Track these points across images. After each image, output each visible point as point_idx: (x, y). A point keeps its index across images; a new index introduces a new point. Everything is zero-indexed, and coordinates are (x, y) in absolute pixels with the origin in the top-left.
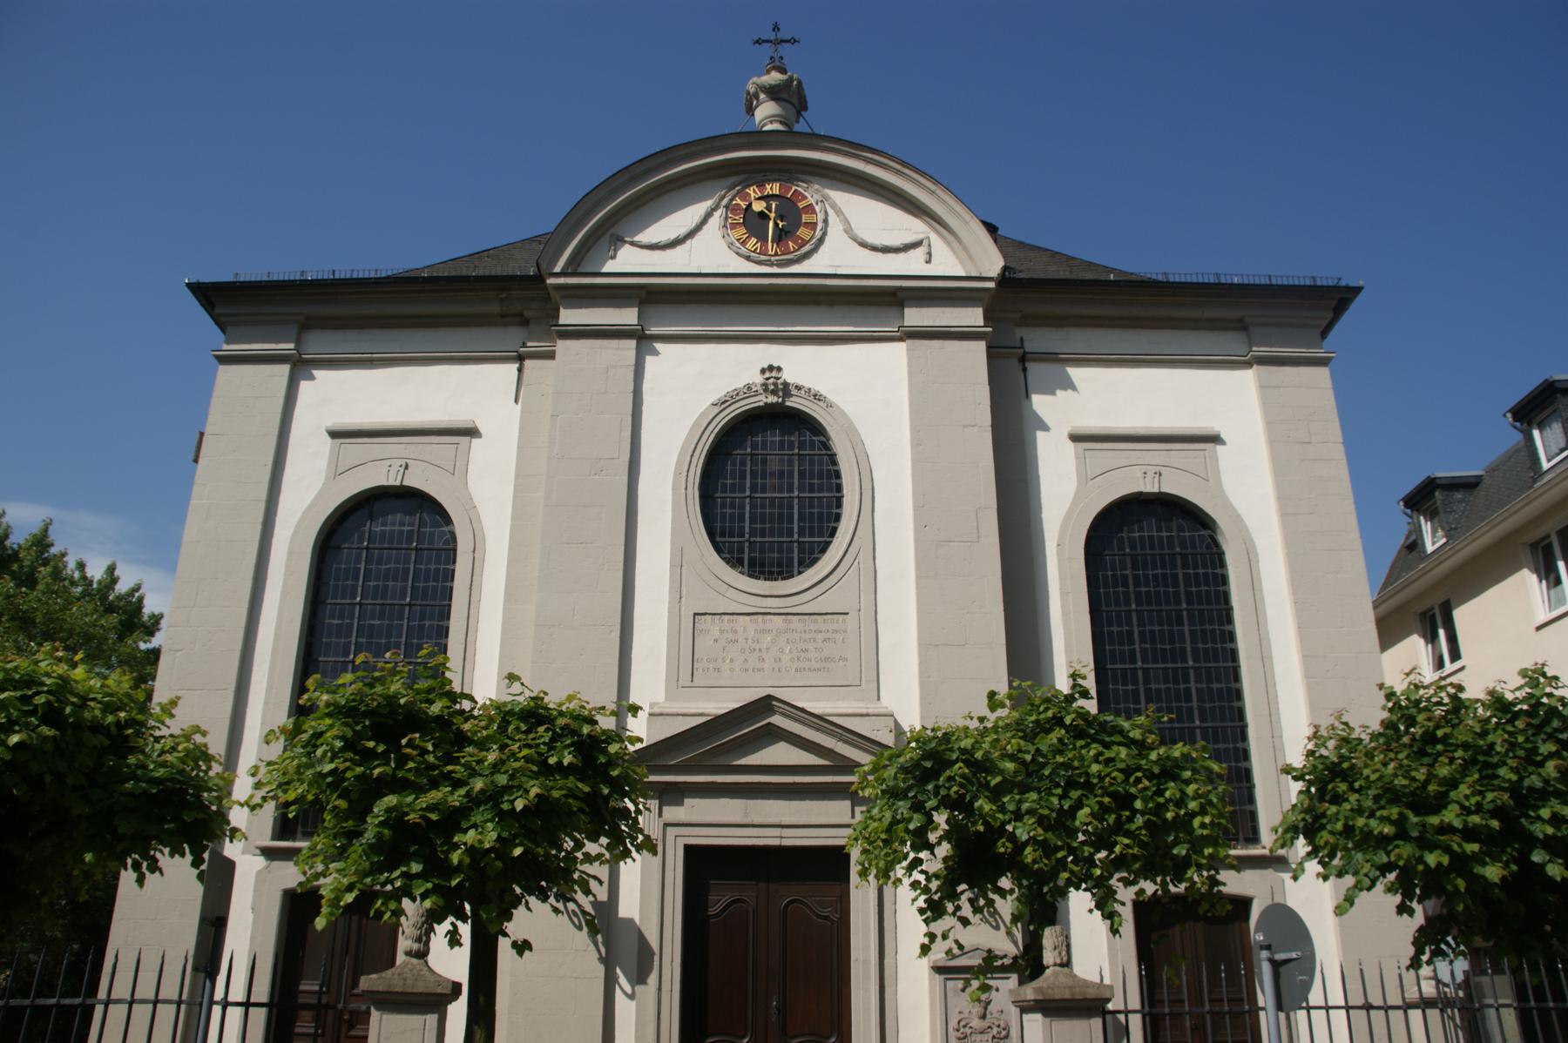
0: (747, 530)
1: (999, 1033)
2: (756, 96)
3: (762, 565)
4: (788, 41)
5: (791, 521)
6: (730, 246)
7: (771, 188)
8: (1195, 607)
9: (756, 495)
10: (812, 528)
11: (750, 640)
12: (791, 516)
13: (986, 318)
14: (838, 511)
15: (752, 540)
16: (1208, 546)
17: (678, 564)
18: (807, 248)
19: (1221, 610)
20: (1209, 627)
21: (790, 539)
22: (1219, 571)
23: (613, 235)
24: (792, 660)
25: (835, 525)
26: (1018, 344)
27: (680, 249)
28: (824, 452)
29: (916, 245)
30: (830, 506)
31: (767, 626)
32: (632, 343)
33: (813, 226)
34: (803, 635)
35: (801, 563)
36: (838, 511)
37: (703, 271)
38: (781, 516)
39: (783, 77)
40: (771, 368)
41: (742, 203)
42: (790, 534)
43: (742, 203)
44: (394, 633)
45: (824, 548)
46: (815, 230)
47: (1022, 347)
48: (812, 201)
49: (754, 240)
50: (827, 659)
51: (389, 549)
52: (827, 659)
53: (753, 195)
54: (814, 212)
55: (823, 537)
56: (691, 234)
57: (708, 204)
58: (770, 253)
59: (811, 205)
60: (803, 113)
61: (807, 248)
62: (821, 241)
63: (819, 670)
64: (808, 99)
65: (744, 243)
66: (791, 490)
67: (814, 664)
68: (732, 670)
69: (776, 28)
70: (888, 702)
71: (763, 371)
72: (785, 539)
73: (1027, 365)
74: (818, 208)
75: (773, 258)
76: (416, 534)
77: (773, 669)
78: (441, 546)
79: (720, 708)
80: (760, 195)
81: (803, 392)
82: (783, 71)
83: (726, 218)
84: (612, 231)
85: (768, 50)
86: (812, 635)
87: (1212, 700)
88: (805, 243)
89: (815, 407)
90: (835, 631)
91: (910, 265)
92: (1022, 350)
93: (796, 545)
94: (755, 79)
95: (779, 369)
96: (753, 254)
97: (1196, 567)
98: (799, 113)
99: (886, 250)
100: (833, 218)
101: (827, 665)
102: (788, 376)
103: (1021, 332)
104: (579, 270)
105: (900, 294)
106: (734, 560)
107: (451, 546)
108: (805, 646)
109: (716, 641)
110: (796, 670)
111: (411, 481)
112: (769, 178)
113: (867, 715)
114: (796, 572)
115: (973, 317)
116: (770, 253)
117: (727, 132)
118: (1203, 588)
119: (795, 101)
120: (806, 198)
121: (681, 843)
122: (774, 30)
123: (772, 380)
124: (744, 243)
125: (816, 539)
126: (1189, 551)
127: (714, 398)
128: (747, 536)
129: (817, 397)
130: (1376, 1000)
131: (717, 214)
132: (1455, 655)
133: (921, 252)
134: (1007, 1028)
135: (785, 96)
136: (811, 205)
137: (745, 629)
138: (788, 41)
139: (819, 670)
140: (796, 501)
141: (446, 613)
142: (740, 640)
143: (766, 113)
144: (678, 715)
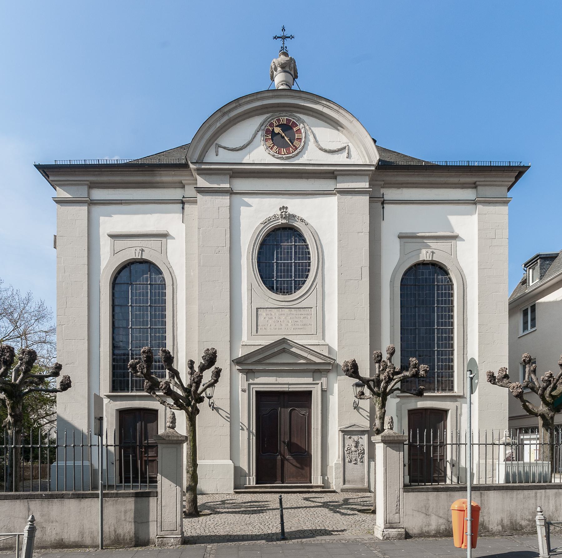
0: (275, 276)
1: (361, 452)
2: (276, 69)
3: (281, 289)
5: (291, 272)
8: (440, 306)
9: (278, 262)
10: (299, 275)
11: (277, 318)
12: (291, 269)
16: (448, 282)
17: (251, 289)
18: (291, 155)
19: (450, 307)
20: (444, 313)
21: (291, 279)
22: (450, 292)
23: (216, 144)
24: (292, 325)
26: (382, 197)
28: (304, 244)
30: (306, 266)
31: (283, 313)
34: (296, 316)
35: (295, 289)
36: (309, 268)
38: (288, 269)
39: (288, 59)
42: (291, 277)
43: (270, 128)
44: (9, 442)
46: (301, 142)
47: (383, 198)
50: (304, 325)
51: (140, 284)
52: (304, 325)
53: (275, 124)
61: (291, 155)
63: (302, 329)
66: (291, 260)
67: (300, 327)
68: (270, 329)
69: (283, 29)
70: (327, 341)
71: (280, 209)
72: (289, 279)
73: (385, 205)
75: (284, 156)
76: (149, 278)
78: (159, 283)
79: (267, 343)
82: (286, 54)
84: (215, 142)
85: (279, 42)
86: (300, 316)
87: (442, 341)
89: (301, 225)
90: (308, 314)
91: (340, 159)
92: (383, 199)
93: (293, 281)
95: (287, 208)
96: (275, 154)
97: (442, 290)
98: (294, 79)
101: (305, 327)
102: (290, 211)
103: (383, 191)
105: (335, 172)
106: (271, 288)
107: (163, 283)
110: (294, 329)
111: (145, 256)
113: (319, 345)
114: (293, 292)
115: (365, 185)
118: (444, 298)
119: (292, 73)
121: (254, 390)
122: (282, 30)
125: (301, 279)
126: (440, 284)
127: (262, 221)
128: (275, 278)
129: (302, 220)
130: (490, 447)
132: (533, 325)
133: (345, 154)
134: (364, 450)
135: (287, 69)
137: (275, 314)
139: (302, 329)
140: (293, 264)
141: (164, 309)
142: (273, 318)
143: (279, 78)
144: (252, 345)
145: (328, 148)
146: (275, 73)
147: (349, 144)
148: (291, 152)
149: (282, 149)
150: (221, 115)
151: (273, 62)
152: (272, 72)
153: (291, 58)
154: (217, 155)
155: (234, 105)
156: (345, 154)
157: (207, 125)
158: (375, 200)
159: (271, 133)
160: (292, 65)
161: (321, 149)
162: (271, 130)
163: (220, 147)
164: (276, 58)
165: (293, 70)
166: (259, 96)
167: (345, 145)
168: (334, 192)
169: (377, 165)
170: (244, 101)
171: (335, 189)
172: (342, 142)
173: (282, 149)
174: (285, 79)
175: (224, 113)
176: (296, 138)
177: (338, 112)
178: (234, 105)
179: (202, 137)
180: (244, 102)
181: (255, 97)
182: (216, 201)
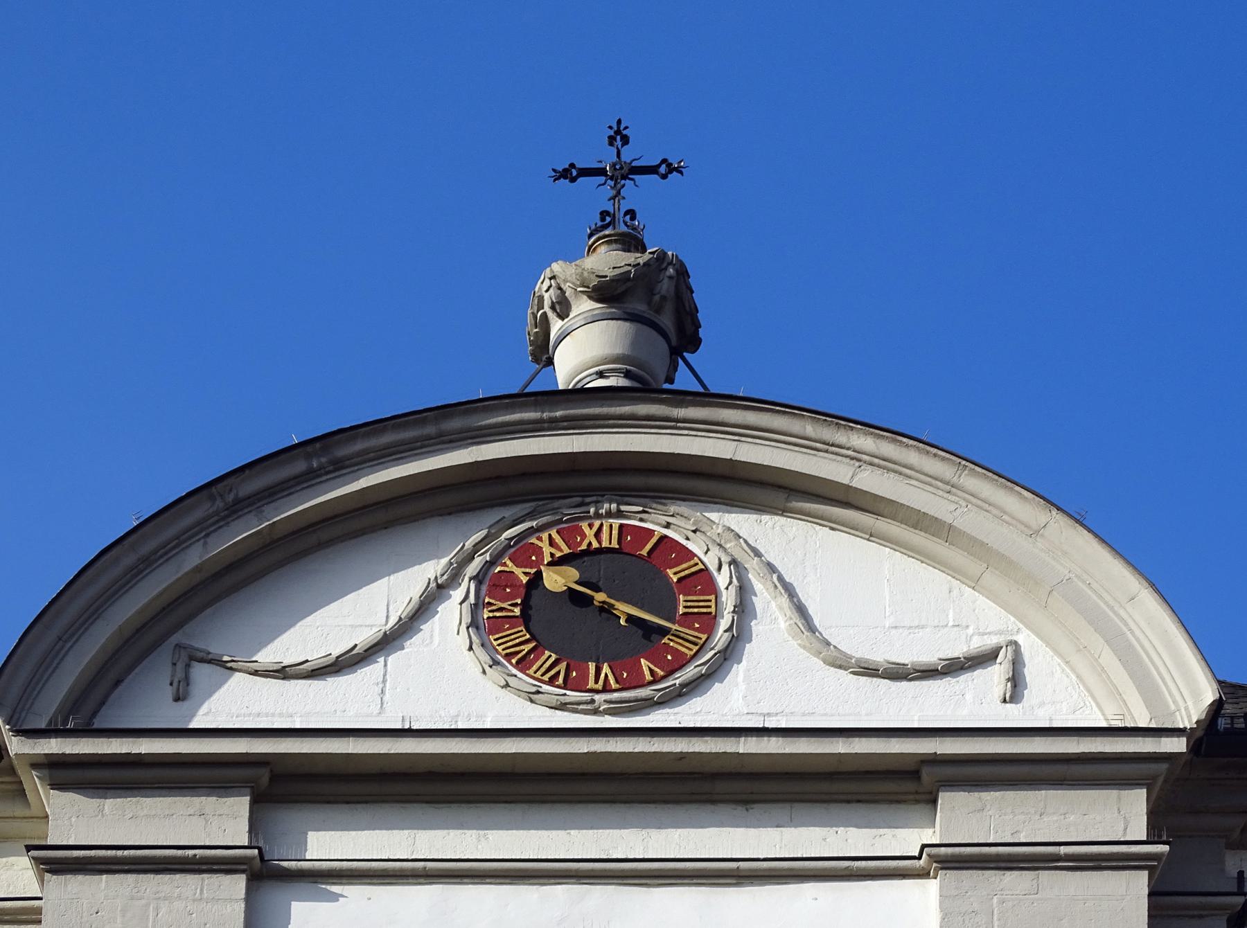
7: (598, 535)
13: (1153, 815)
18: (689, 672)
27: (369, 674)
32: (237, 885)
33: (709, 622)
41: (518, 571)
43: (518, 571)
53: (547, 550)
56: (387, 642)
57: (432, 569)
58: (591, 684)
61: (689, 672)
62: (729, 654)
69: (619, 136)
75: (597, 697)
80: (566, 550)
82: (631, 242)
83: (475, 609)
85: (597, 194)
88: (681, 662)
99: (898, 673)
100: (766, 599)
104: (97, 724)
116: (591, 684)
120: (692, 555)
122: (612, 140)
131: (457, 594)
133: (996, 675)
145: (879, 655)
146: (556, 326)
147: (1020, 639)
148: (648, 677)
149: (592, 667)
150: (217, 513)
151: (548, 273)
152: (545, 324)
153: (661, 257)
154: (177, 699)
155: (299, 466)
156: (996, 675)
157: (129, 560)
158: (1187, 907)
159: (523, 591)
160: (665, 287)
161: (840, 662)
162: (525, 579)
163: (202, 661)
164: (570, 258)
165: (669, 308)
166: (456, 423)
167: (991, 641)
168: (922, 862)
169: (1199, 733)
170: (359, 446)
171: (924, 846)
172: (970, 631)
173: (592, 667)
174: (618, 350)
175: (238, 501)
176: (681, 610)
177: (830, 447)
178: (299, 466)
179: (94, 613)
180: (359, 454)
181: (430, 430)
182: (157, 910)
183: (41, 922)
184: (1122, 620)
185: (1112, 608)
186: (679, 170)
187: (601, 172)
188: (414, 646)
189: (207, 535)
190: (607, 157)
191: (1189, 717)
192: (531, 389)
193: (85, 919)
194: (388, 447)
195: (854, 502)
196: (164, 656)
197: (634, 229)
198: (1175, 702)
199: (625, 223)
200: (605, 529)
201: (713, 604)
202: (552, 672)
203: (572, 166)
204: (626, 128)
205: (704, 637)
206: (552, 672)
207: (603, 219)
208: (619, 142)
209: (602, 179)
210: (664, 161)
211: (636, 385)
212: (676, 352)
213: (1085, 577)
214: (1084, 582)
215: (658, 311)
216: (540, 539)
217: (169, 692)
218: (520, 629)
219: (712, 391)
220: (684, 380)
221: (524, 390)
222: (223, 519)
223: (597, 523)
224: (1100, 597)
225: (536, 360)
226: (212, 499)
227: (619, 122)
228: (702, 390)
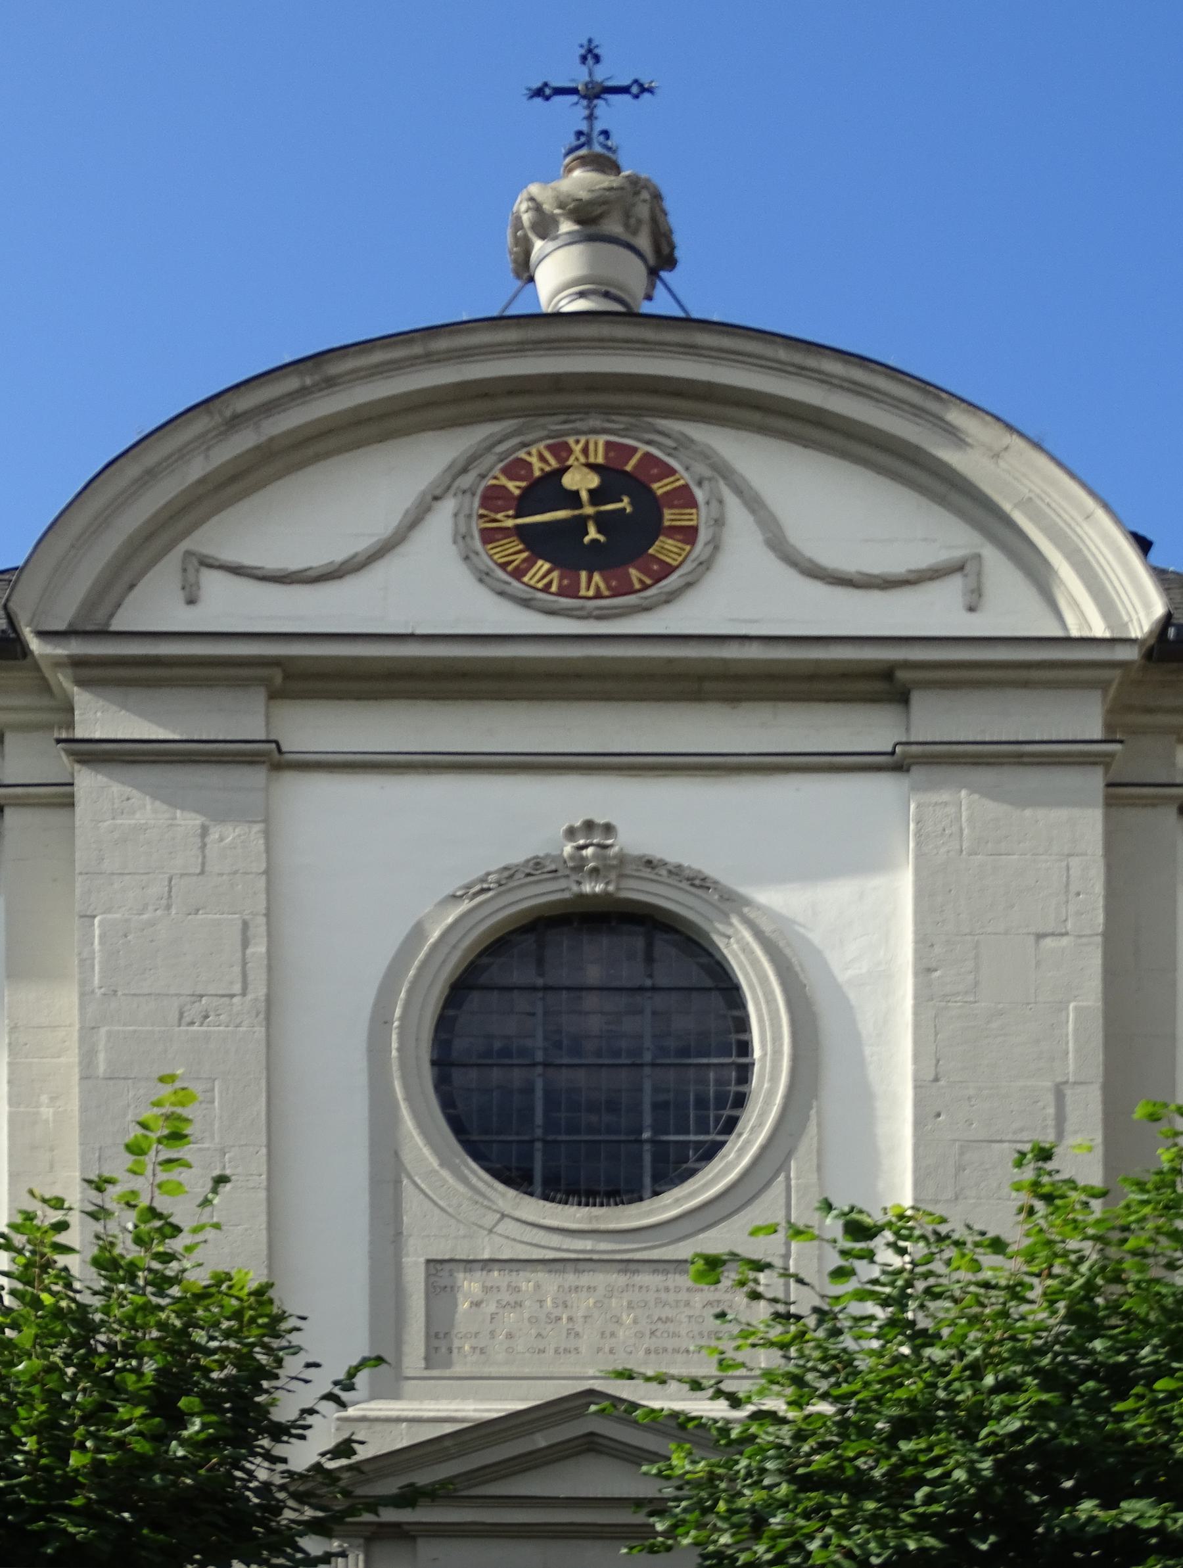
4: (624, 90)
6: (483, 577)
14: (741, 1089)
15: (550, 1138)
24: (640, 1335)
25: (734, 1113)
29: (958, 568)
34: (663, 1296)
37: (419, 631)
40: (589, 826)
45: (710, 1152)
48: (685, 478)
49: (543, 566)
54: (692, 503)
55: (707, 1133)
57: (305, 574)
58: (583, 592)
59: (686, 487)
60: (663, 274)
62: (706, 565)
64: (677, 238)
65: (518, 574)
69: (590, 55)
71: (571, 833)
74: (700, 495)
77: (603, 1333)
81: (664, 872)
82: (605, 163)
88: (668, 570)
94: (534, 189)
95: (608, 829)
100: (735, 509)
105: (901, 675)
108: (667, 1312)
109: (477, 1304)
110: (648, 1351)
112: (578, 425)
116: (583, 592)
117: (465, 318)
119: (643, 242)
120: (672, 472)
122: (584, 59)
123: (589, 851)
124: (518, 574)
129: (700, 883)
135: (614, 227)
136: (686, 487)
138: (624, 90)
148: (637, 586)
149: (584, 575)
159: (515, 503)
164: (546, 180)
166: (442, 344)
180: (353, 371)
181: (417, 349)
183: (72, 805)
184: (1079, 536)
185: (1069, 526)
186: (650, 90)
187: (573, 91)
188: (409, 548)
189: (208, 449)
190: (579, 76)
191: (1141, 627)
192: (509, 313)
193: (116, 806)
194: (377, 366)
195: (1046, 446)
196: (171, 563)
197: (609, 149)
198: (1128, 613)
199: (600, 144)
200: (591, 447)
201: (694, 517)
202: (545, 581)
203: (546, 85)
204: (597, 46)
205: (688, 548)
206: (545, 581)
207: (578, 139)
208: (590, 61)
209: (575, 98)
210: (636, 81)
211: (618, 307)
212: (653, 273)
213: (1043, 496)
214: (1043, 500)
215: (635, 233)
216: (529, 454)
217: (180, 596)
218: (512, 539)
219: (695, 315)
220: (661, 305)
221: (504, 311)
222: (221, 434)
223: (583, 440)
224: (1059, 516)
225: (518, 276)
226: (210, 413)
227: (590, 41)
228: (681, 314)
